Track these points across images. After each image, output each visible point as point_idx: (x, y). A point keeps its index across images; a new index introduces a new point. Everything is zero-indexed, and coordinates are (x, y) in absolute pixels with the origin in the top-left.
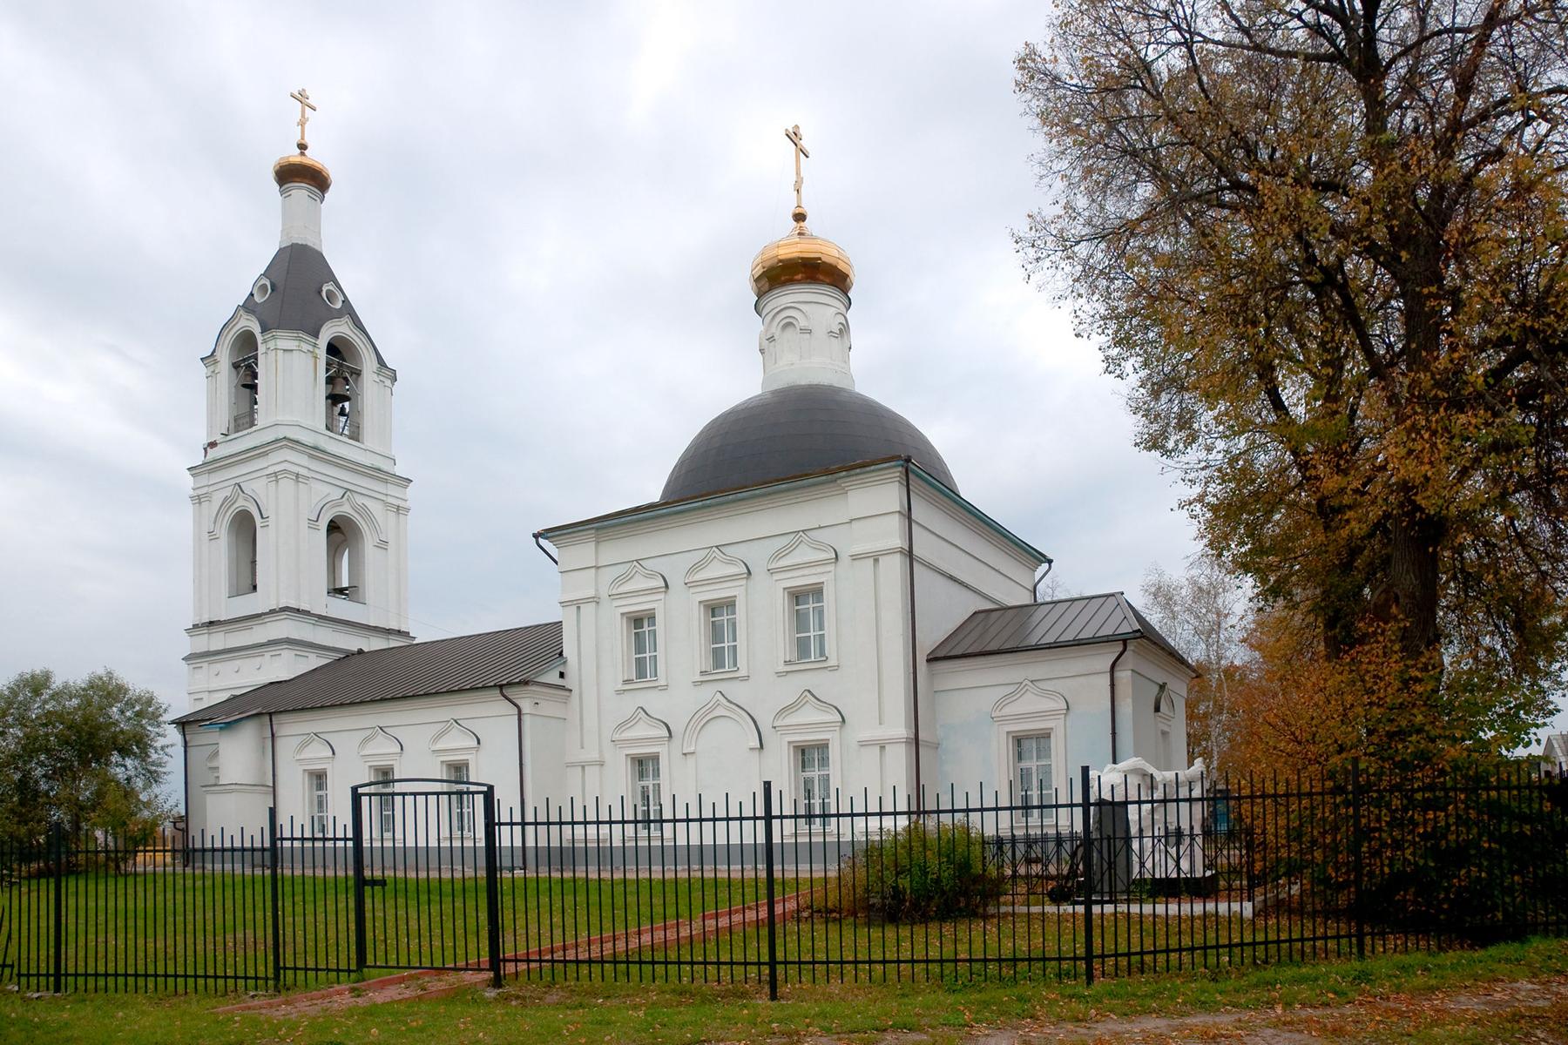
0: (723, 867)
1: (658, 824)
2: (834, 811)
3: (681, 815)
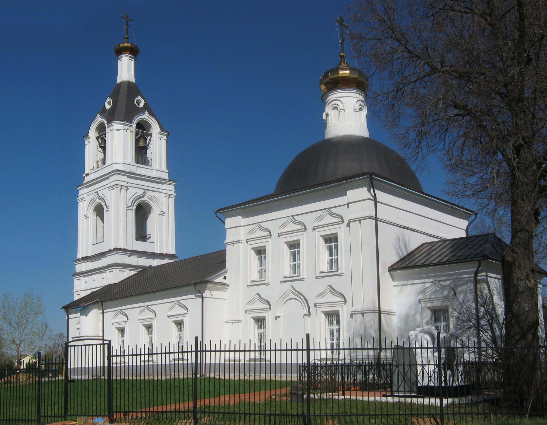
0: (273, 375)
3: (223, 349)
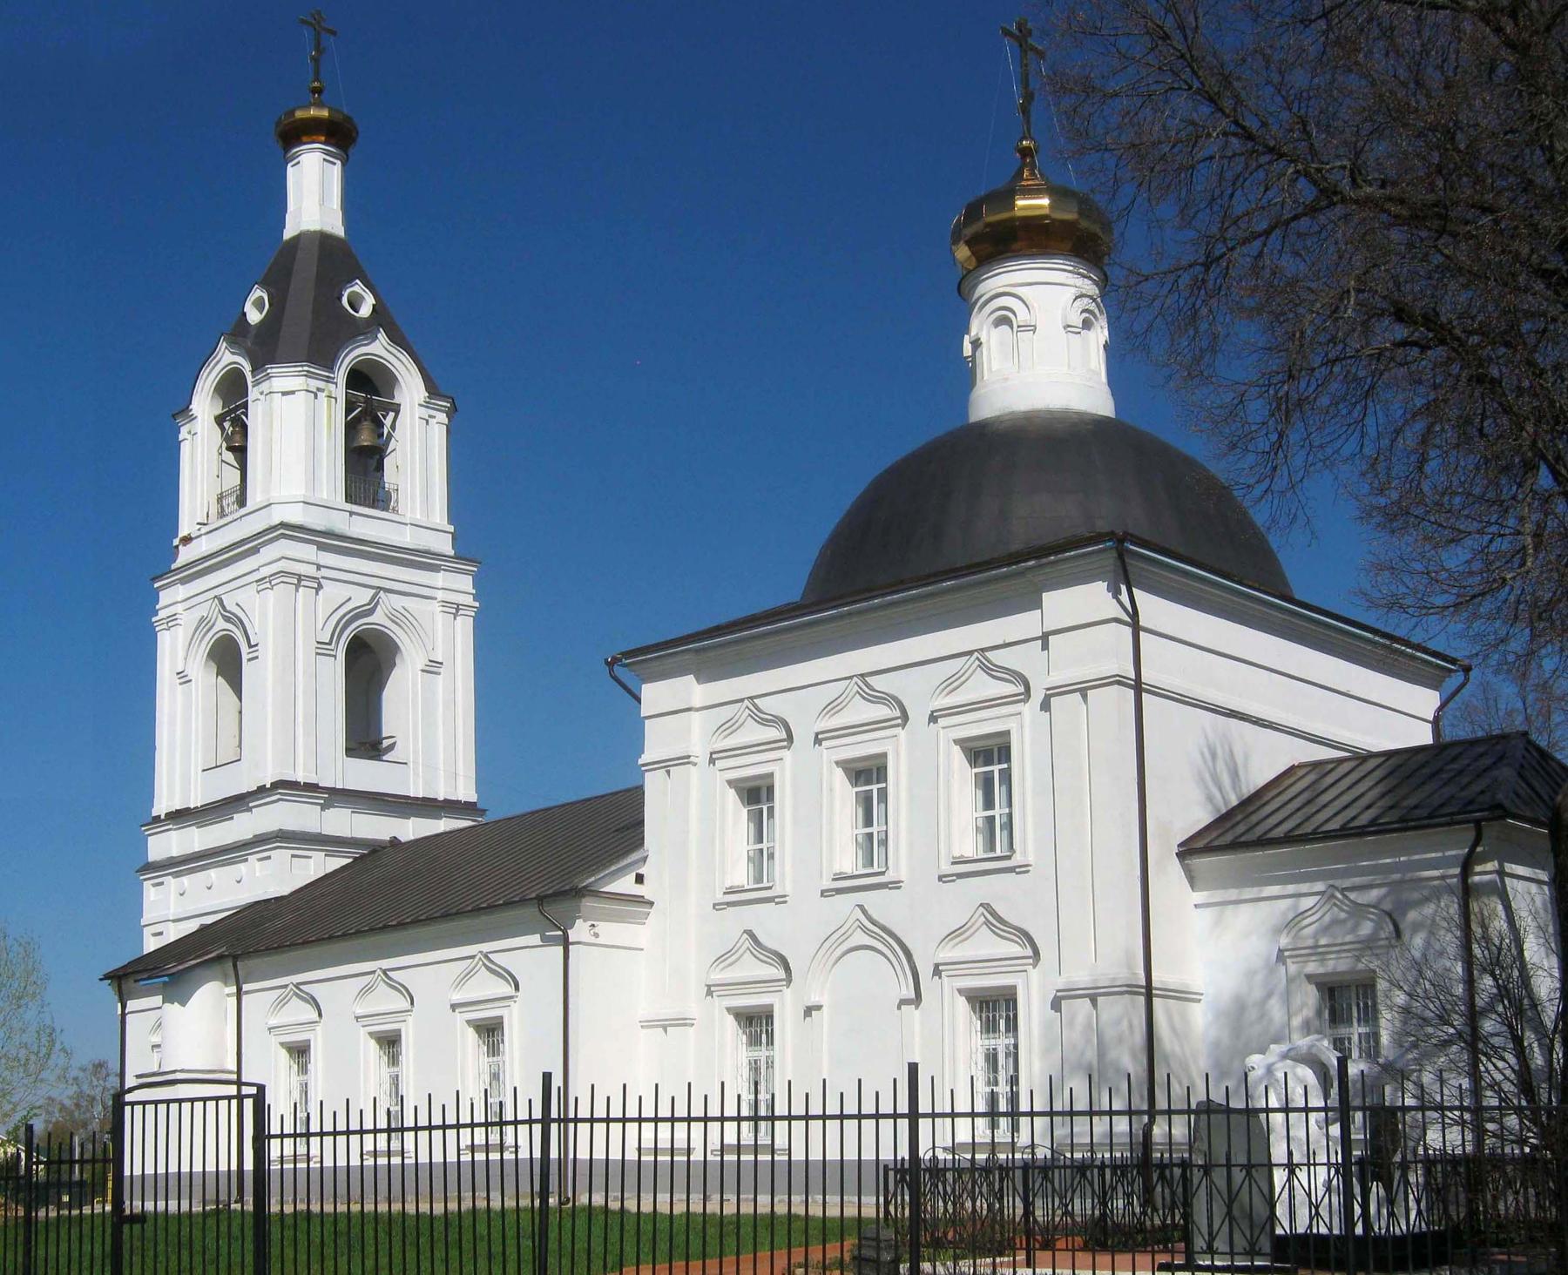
1: (1095, 1108)
2: (745, 1125)
